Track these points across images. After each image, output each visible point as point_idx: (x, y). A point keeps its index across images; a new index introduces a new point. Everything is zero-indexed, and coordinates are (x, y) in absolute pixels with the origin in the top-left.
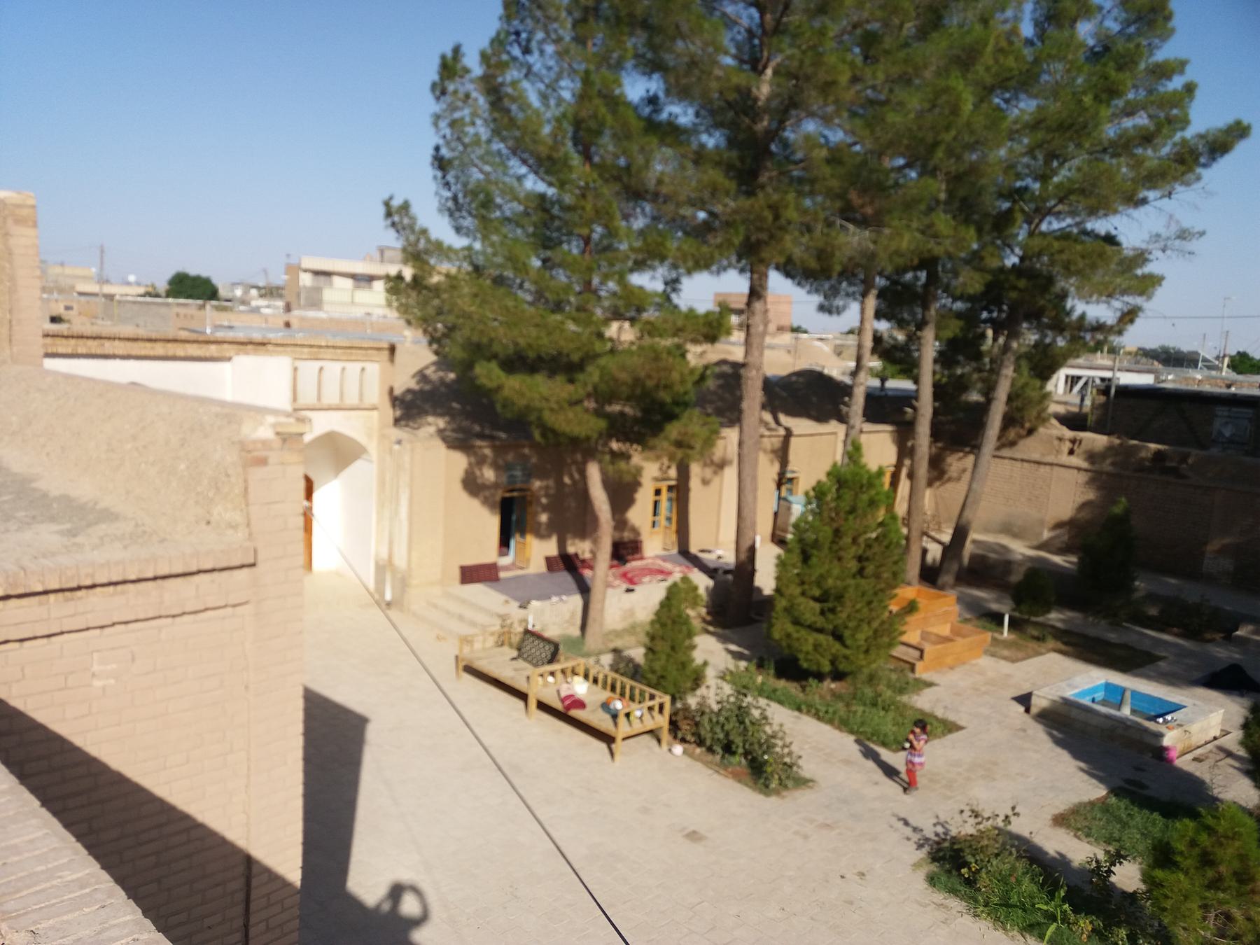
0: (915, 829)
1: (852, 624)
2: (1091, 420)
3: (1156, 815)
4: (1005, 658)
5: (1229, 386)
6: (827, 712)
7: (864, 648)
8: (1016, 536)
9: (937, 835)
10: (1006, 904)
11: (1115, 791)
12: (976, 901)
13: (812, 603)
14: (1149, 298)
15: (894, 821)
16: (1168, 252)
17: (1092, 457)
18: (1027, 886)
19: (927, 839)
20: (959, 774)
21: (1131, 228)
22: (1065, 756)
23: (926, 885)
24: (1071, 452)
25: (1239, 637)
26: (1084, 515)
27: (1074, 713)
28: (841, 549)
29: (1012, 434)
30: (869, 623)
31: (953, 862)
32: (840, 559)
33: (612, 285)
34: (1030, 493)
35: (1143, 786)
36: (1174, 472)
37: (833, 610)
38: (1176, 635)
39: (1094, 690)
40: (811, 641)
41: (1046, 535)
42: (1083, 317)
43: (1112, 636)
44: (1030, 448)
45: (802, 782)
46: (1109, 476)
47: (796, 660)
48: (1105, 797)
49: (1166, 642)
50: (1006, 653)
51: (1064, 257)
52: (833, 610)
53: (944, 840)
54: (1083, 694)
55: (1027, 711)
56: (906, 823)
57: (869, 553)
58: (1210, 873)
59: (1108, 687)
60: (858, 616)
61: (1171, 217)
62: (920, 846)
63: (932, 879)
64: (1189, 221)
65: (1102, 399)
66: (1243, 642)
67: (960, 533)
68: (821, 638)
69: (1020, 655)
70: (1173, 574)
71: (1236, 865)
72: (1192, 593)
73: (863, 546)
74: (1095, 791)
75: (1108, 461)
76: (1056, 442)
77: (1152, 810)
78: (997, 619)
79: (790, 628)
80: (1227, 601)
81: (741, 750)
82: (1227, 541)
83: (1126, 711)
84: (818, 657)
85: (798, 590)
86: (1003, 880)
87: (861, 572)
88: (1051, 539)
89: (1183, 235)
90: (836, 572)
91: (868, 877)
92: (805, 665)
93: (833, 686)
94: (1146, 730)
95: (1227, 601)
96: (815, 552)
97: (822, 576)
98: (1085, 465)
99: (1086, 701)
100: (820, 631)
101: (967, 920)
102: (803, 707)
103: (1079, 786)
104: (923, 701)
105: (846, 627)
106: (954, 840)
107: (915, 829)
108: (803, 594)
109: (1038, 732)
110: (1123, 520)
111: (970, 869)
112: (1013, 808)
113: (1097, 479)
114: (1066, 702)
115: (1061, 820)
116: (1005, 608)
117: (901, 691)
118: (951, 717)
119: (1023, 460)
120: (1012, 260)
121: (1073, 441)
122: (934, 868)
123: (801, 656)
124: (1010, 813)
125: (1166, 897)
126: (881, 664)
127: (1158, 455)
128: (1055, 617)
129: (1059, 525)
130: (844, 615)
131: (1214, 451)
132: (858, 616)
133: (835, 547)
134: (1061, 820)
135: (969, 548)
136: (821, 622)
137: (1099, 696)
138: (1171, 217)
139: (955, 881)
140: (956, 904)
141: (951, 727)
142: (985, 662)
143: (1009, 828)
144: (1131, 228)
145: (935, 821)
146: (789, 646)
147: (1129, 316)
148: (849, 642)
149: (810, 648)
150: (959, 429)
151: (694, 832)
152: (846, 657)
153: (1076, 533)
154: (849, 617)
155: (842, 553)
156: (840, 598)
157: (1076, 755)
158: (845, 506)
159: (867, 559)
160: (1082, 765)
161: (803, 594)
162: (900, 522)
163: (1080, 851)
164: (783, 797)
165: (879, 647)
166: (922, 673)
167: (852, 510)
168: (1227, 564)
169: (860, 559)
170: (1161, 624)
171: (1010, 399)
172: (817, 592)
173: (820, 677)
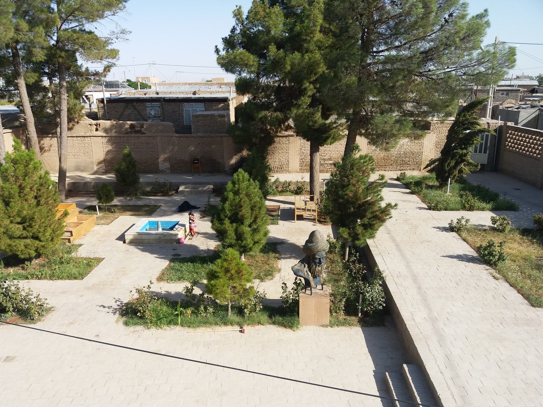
0: (109, 308)
1: (41, 230)
2: (100, 114)
3: (189, 263)
4: (103, 224)
5: (145, 94)
6: (42, 275)
7: (50, 239)
8: (82, 171)
9: (118, 306)
10: (159, 319)
11: (172, 260)
12: (147, 323)
13: (17, 226)
14: (118, 59)
15: (98, 308)
16: (119, 39)
17: (106, 130)
18: (165, 308)
19: (116, 309)
20: (113, 277)
21: (101, 28)
22: (147, 254)
23: (124, 327)
24: (97, 130)
25: (181, 191)
26: (110, 156)
27: (144, 237)
28: (26, 195)
29: (71, 125)
30: (50, 226)
31: (131, 312)
32: (26, 200)
33: (333, 87)
34: (84, 150)
35: (179, 255)
36: (139, 132)
37: (30, 226)
38: (160, 196)
39: (146, 226)
40: (22, 244)
41: (96, 168)
42: (87, 69)
43: (140, 203)
44: (79, 130)
45: (49, 310)
46: (116, 138)
47: (17, 256)
48: (169, 265)
49: (158, 199)
50: (102, 222)
51: (81, 41)
52: (30, 226)
53: (123, 306)
54: (142, 229)
55: (124, 242)
56: (104, 307)
57: (40, 193)
58: (229, 275)
59: (150, 223)
60: (44, 225)
61: (117, 24)
62: (115, 313)
63: (126, 323)
64: (125, 26)
65: (102, 105)
66: (182, 192)
67: (62, 174)
68: (28, 241)
69: (109, 221)
70: (150, 173)
71: (236, 269)
72: (161, 179)
73: (36, 191)
74: (165, 263)
75: (114, 131)
76: (89, 126)
77: (187, 262)
78: (92, 209)
79: (8, 241)
80: (173, 179)
81: (11, 309)
82: (166, 156)
83: (160, 231)
84: (29, 250)
85: (9, 221)
86: (155, 310)
87: (38, 204)
88: (99, 169)
89: (123, 32)
90: (26, 207)
91: (100, 336)
92: (23, 257)
93: (37, 261)
94: (172, 234)
95: (173, 179)
96: (11, 200)
97: (19, 211)
98: (104, 134)
99: (144, 231)
100: (26, 238)
101: (147, 331)
102: (29, 276)
103: (159, 264)
104: (82, 253)
105: (39, 232)
106: (127, 304)
107: (109, 308)
108: (11, 222)
109: (133, 249)
110: (128, 155)
111: (140, 312)
112: (151, 281)
113: (112, 140)
114: (139, 234)
115: (160, 279)
116: (95, 202)
117: (69, 252)
118: (97, 255)
119: (77, 137)
120: (53, 42)
121: (96, 125)
122: (124, 319)
123: (19, 253)
124: (149, 284)
125: (218, 289)
126: (58, 245)
127: (132, 126)
128: (116, 201)
129: (99, 163)
130: (37, 227)
131: (150, 121)
132: (44, 225)
133: (22, 195)
134: (160, 279)
135: (68, 181)
136: (25, 233)
137: (148, 227)
138: (117, 24)
139: (136, 320)
140: (139, 328)
141: (99, 260)
142: (97, 228)
143: (151, 290)
144: (101, 28)
145: (115, 300)
146: (11, 250)
147: (107, 69)
148: (42, 239)
149: (23, 248)
150: (48, 126)
151: (8, 357)
152: (43, 247)
153: (108, 164)
154: (40, 226)
155: (26, 197)
156: (32, 219)
157: (152, 253)
158: (20, 173)
159: (40, 196)
160: (156, 255)
161: (11, 222)
162: (382, 173)
163: (178, 287)
164: (43, 320)
165: (58, 236)
166: (75, 241)
167: (26, 175)
168: (167, 165)
169: (36, 197)
170: (154, 193)
171: (69, 110)
172: (19, 220)
173: (30, 259)
